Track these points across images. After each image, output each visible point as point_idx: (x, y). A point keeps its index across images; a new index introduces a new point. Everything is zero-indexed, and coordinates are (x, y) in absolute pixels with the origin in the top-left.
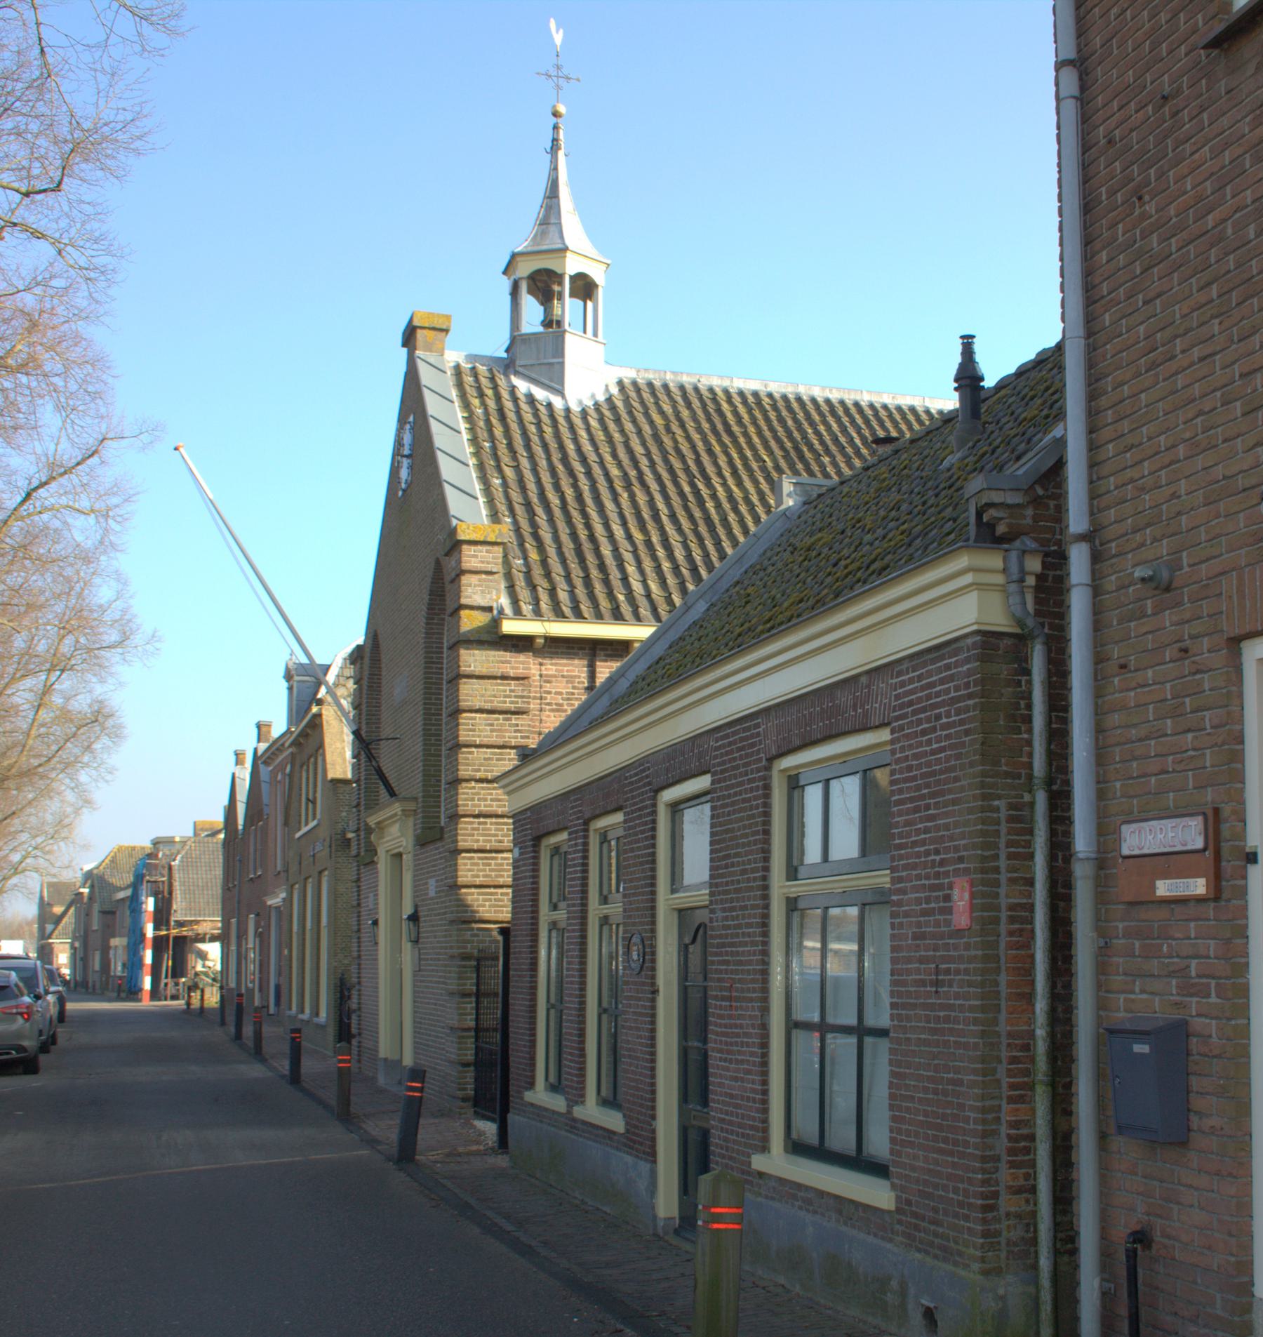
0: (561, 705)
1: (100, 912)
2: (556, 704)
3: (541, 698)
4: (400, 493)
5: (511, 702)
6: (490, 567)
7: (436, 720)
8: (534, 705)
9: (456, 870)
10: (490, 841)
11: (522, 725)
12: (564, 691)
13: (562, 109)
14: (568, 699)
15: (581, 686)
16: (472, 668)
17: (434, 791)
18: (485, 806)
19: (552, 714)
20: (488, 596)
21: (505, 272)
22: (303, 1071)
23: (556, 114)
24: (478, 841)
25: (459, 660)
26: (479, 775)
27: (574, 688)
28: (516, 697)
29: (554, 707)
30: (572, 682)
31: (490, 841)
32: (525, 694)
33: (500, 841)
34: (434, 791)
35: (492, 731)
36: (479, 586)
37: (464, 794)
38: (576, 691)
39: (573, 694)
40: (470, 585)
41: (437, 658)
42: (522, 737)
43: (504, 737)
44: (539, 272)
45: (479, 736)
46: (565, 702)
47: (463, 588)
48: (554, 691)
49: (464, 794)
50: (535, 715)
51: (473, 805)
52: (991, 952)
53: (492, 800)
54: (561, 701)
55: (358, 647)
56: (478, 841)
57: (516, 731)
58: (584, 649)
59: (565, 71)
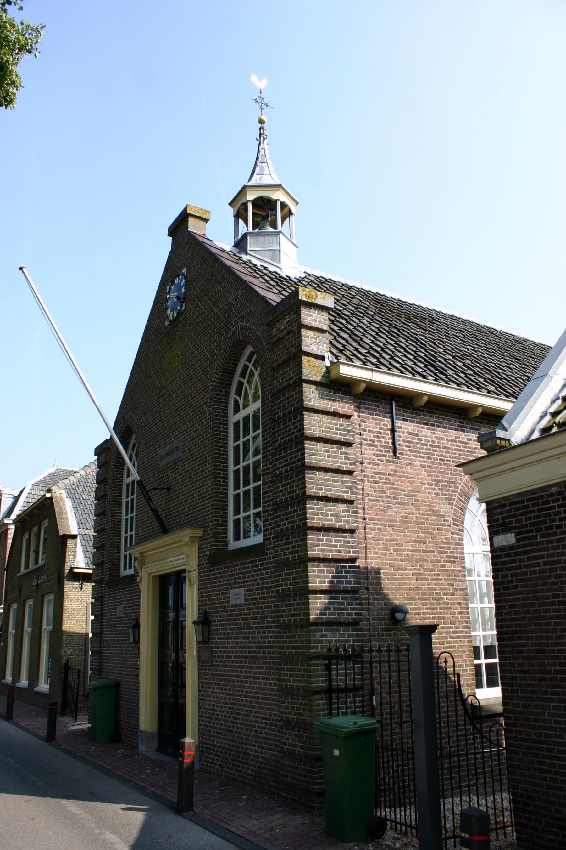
0: (374, 441)
1: (197, 641)
2: (370, 440)
3: (360, 434)
4: (167, 323)
5: (342, 435)
6: (320, 326)
7: (223, 466)
8: (357, 439)
9: (307, 577)
10: (332, 551)
11: (350, 454)
12: (374, 430)
13: (264, 118)
14: (378, 437)
15: (385, 427)
16: (312, 403)
17: (223, 521)
18: (327, 520)
19: (368, 448)
20: (321, 347)
21: (230, 204)
22: (45, 721)
23: (261, 122)
24: (323, 550)
25: (302, 395)
26: (321, 493)
27: (381, 428)
28: (344, 430)
29: (369, 442)
30: (380, 424)
31: (332, 551)
32: (350, 428)
33: (339, 552)
34: (223, 521)
35: (329, 456)
36: (314, 338)
37: (310, 508)
38: (382, 431)
39: (381, 433)
40: (308, 337)
41: (223, 420)
42: (350, 464)
43: (338, 462)
44: (261, 198)
45: (320, 460)
46: (376, 439)
47: (303, 338)
48: (368, 429)
49: (310, 508)
50: (357, 447)
51: (318, 519)
52: (529, 635)
53: (331, 515)
54: (373, 438)
55: (106, 440)
56: (323, 550)
57: (346, 458)
58: (385, 399)
59: (266, 101)
